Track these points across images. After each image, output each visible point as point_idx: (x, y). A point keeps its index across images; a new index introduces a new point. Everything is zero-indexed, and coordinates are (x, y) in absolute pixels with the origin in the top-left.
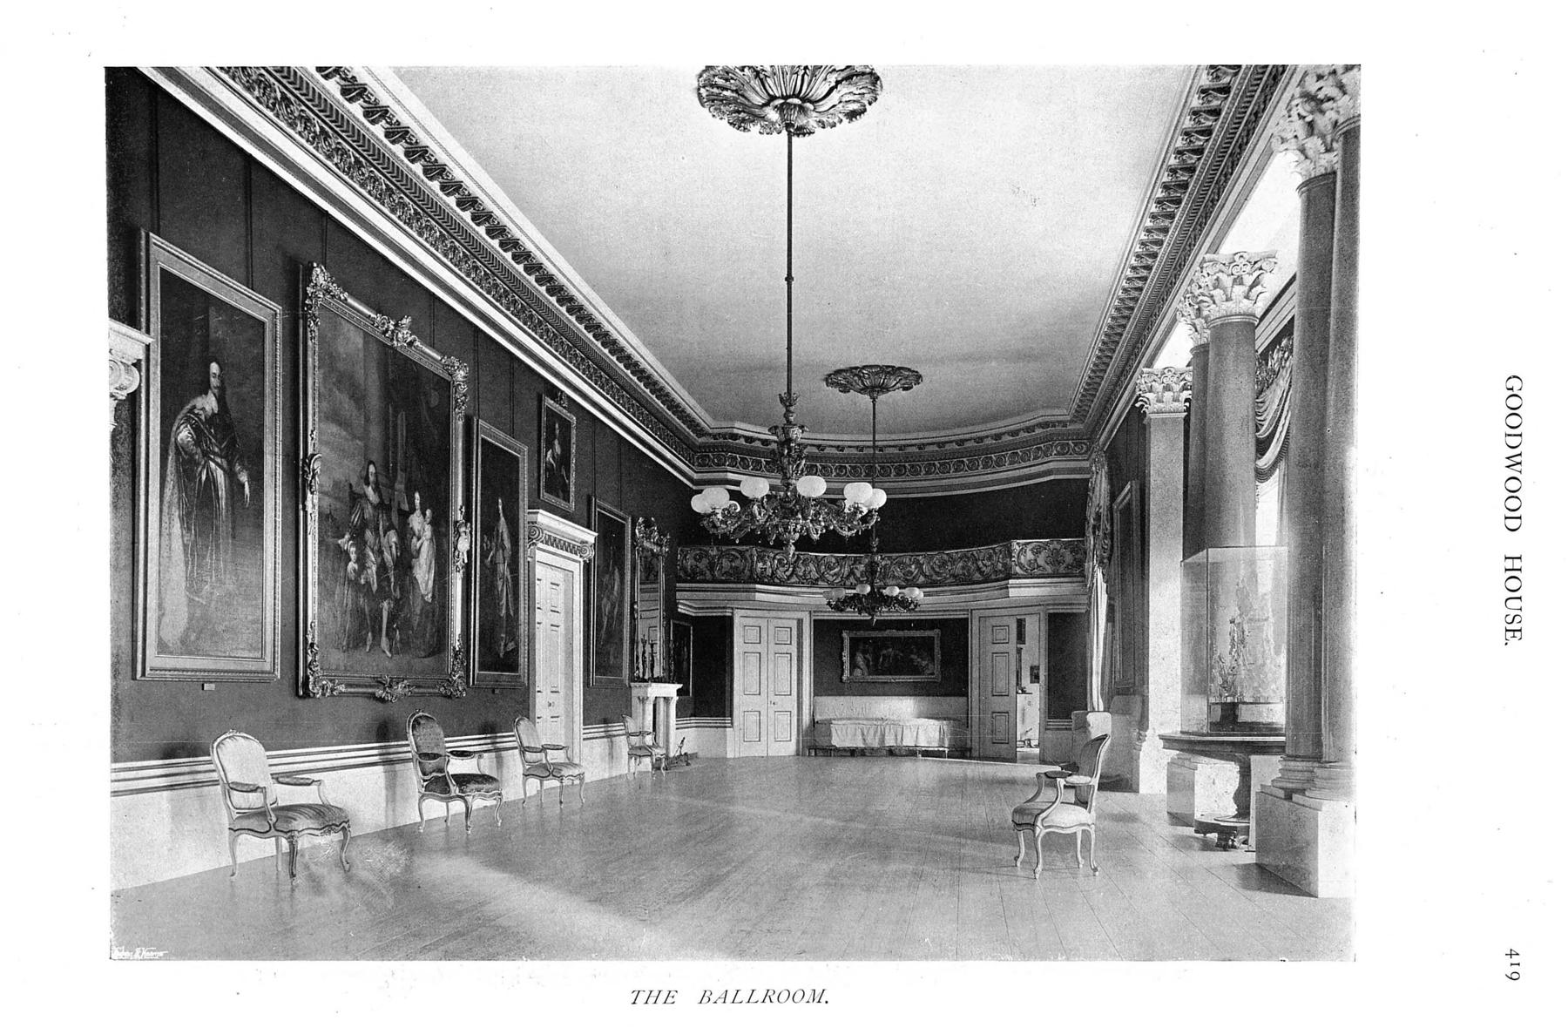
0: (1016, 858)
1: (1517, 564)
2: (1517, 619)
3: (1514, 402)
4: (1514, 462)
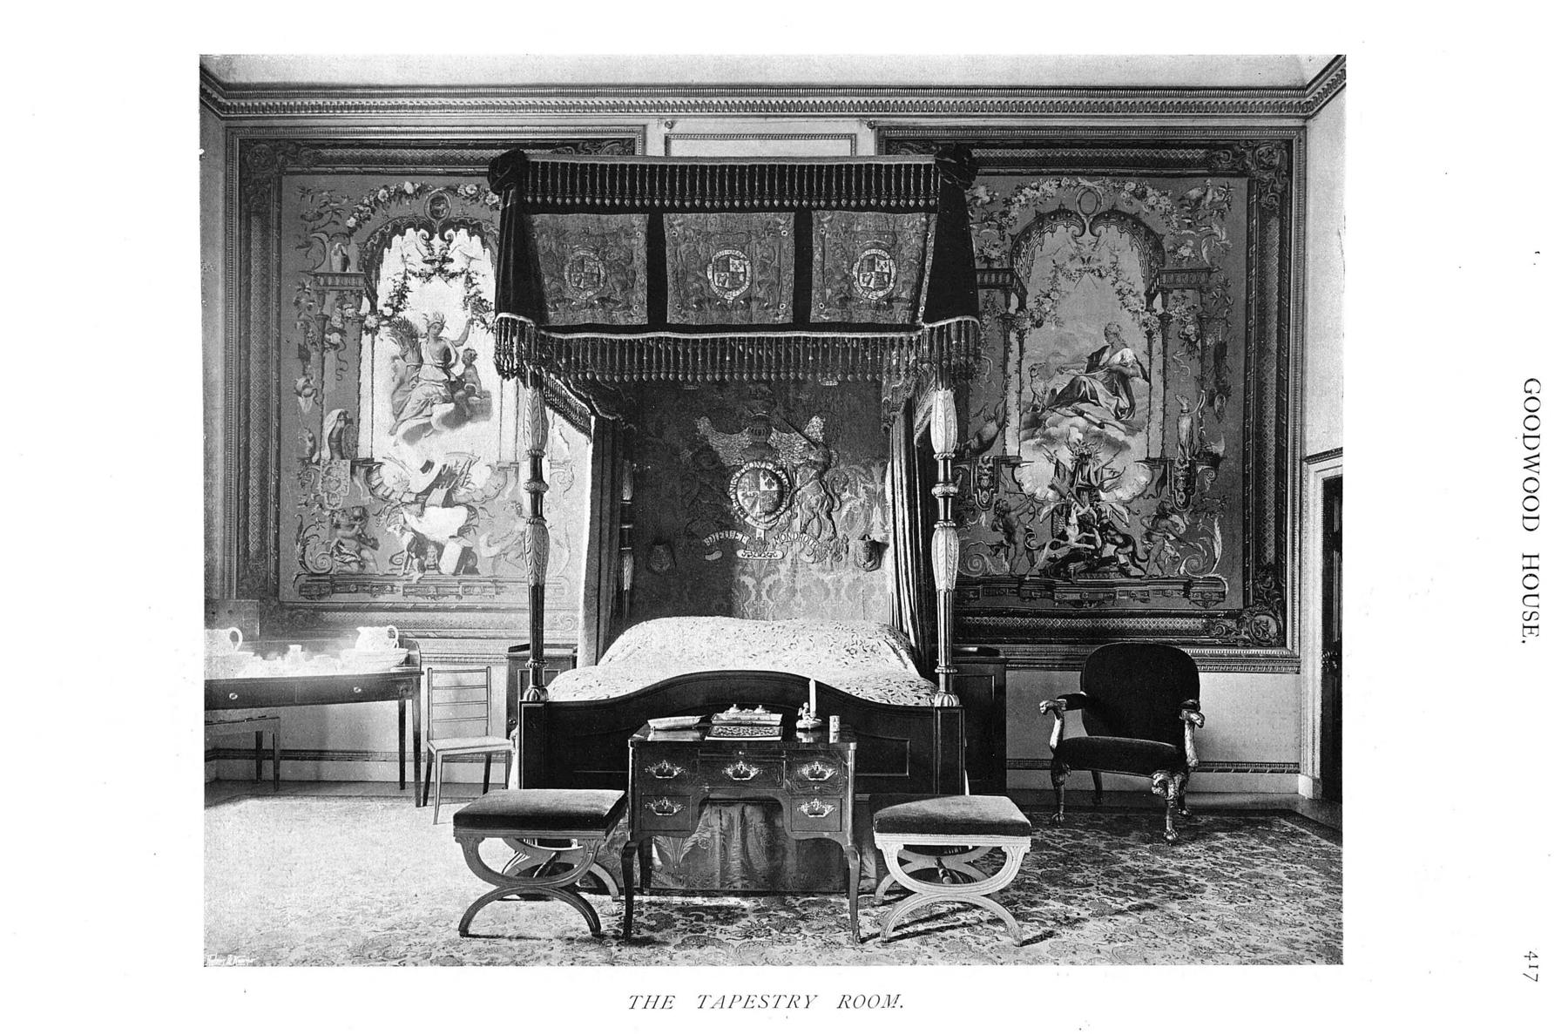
1: (1535, 562)
2: (1535, 616)
3: (1532, 405)
4: (1532, 463)
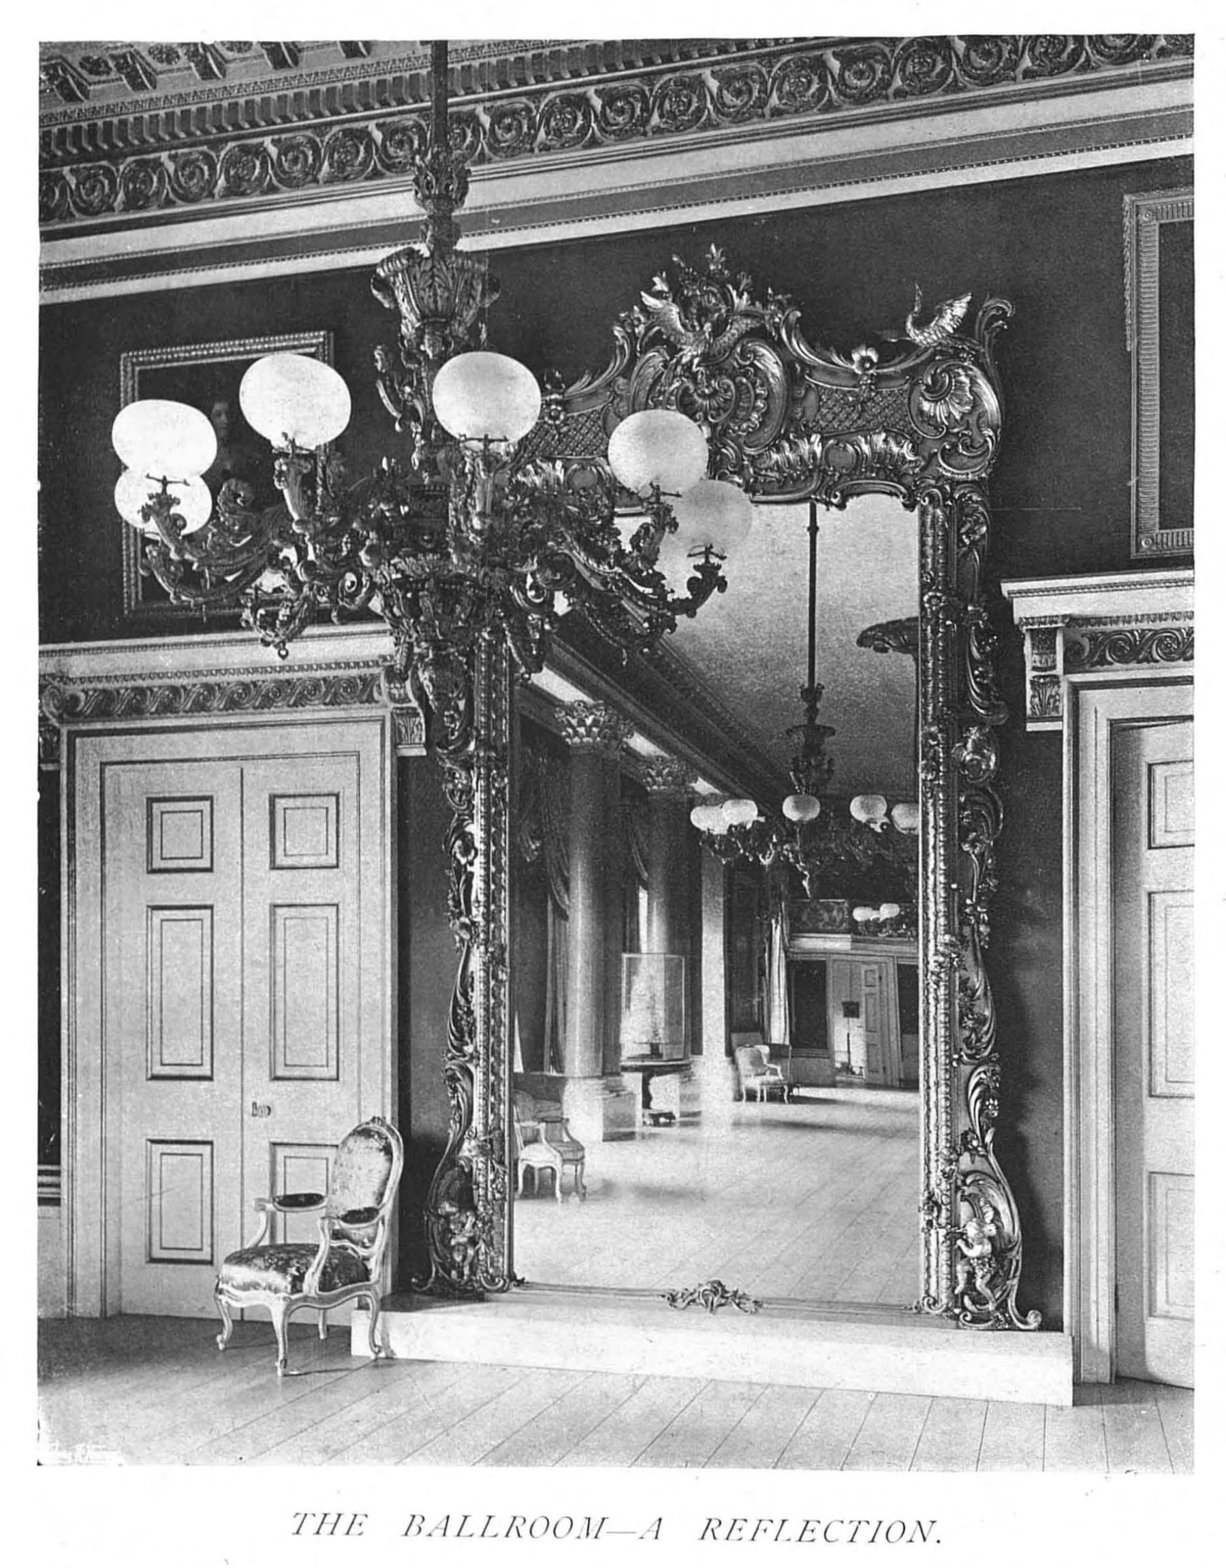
0: (285, 1361)
